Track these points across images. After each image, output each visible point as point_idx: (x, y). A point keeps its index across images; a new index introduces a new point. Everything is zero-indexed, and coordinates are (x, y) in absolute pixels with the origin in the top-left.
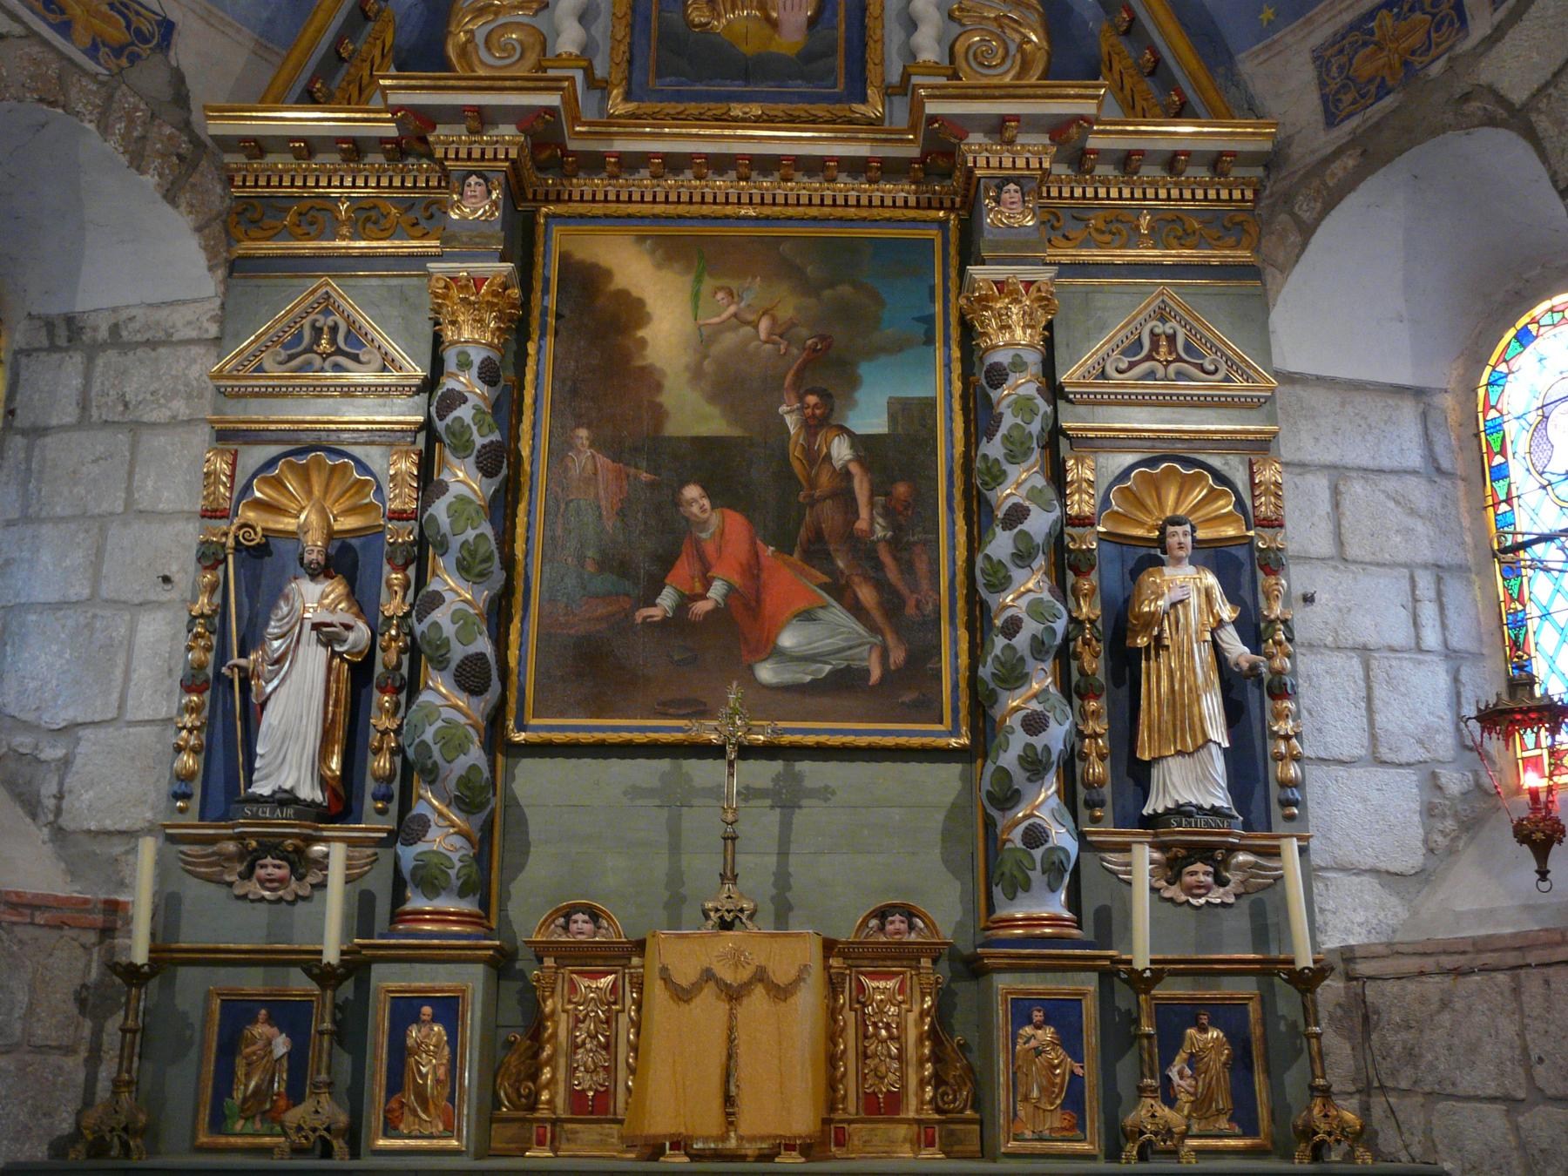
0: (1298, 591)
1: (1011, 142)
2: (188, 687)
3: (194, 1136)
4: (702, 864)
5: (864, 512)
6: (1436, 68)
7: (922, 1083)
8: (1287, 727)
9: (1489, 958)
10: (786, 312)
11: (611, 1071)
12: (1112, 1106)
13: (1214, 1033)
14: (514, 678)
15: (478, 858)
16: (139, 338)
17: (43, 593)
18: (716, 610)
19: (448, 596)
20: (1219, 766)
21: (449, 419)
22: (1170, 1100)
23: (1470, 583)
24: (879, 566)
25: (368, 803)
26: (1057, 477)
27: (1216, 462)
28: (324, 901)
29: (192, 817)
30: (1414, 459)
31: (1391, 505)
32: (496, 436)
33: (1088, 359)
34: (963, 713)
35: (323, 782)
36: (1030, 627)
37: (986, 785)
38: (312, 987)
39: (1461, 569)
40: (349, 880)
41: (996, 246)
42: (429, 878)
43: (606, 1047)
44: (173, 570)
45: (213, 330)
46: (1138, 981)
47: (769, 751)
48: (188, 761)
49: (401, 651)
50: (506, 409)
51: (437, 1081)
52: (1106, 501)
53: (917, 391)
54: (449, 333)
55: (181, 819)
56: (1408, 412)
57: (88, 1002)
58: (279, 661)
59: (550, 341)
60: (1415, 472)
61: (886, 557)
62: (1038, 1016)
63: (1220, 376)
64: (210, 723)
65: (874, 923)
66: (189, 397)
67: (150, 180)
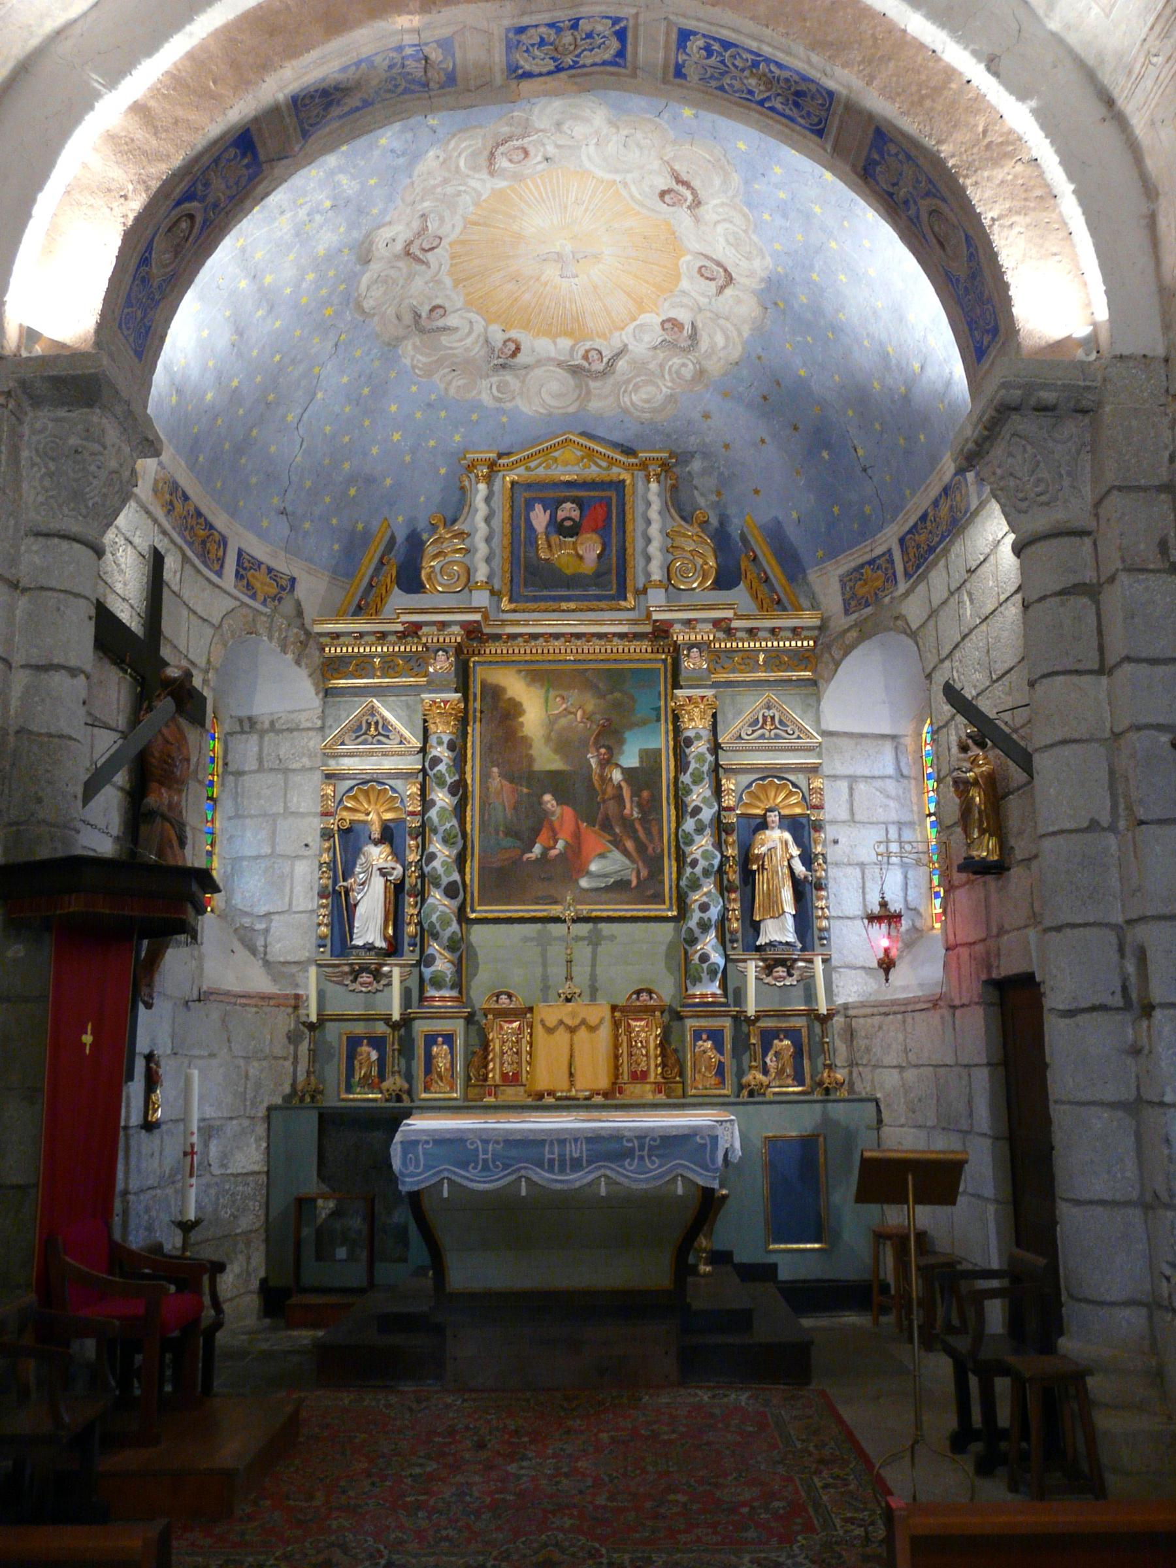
0: (830, 837)
1: (694, 628)
2: (322, 895)
3: (339, 1095)
4: (557, 971)
5: (628, 805)
6: (887, 600)
7: (657, 1066)
8: (822, 904)
9: (896, 1008)
10: (590, 707)
11: (519, 1064)
12: (740, 1073)
13: (787, 1042)
14: (469, 889)
15: (457, 971)
16: (284, 727)
17: (248, 852)
18: (561, 853)
19: (439, 854)
20: (790, 922)
21: (435, 771)
22: (765, 1072)
23: (915, 830)
24: (635, 831)
25: (406, 948)
26: (718, 791)
27: (792, 778)
28: (391, 992)
29: (327, 956)
30: (890, 770)
31: (878, 793)
32: (457, 777)
33: (733, 731)
34: (674, 900)
35: (385, 938)
36: (702, 864)
37: (683, 935)
38: (389, 1030)
39: (911, 824)
40: (401, 982)
41: (688, 679)
42: (437, 983)
43: (517, 1053)
44: (309, 840)
45: (319, 723)
46: (751, 1022)
47: (587, 920)
48: (324, 929)
49: (417, 878)
50: (460, 762)
51: (446, 1069)
52: (741, 798)
53: (652, 745)
54: (432, 728)
55: (322, 957)
56: (888, 748)
57: (293, 1038)
58: (363, 884)
59: (478, 724)
60: (890, 777)
61: (638, 826)
62: (704, 1036)
63: (795, 736)
64: (332, 912)
65: (634, 996)
66: (310, 756)
67: (290, 656)
